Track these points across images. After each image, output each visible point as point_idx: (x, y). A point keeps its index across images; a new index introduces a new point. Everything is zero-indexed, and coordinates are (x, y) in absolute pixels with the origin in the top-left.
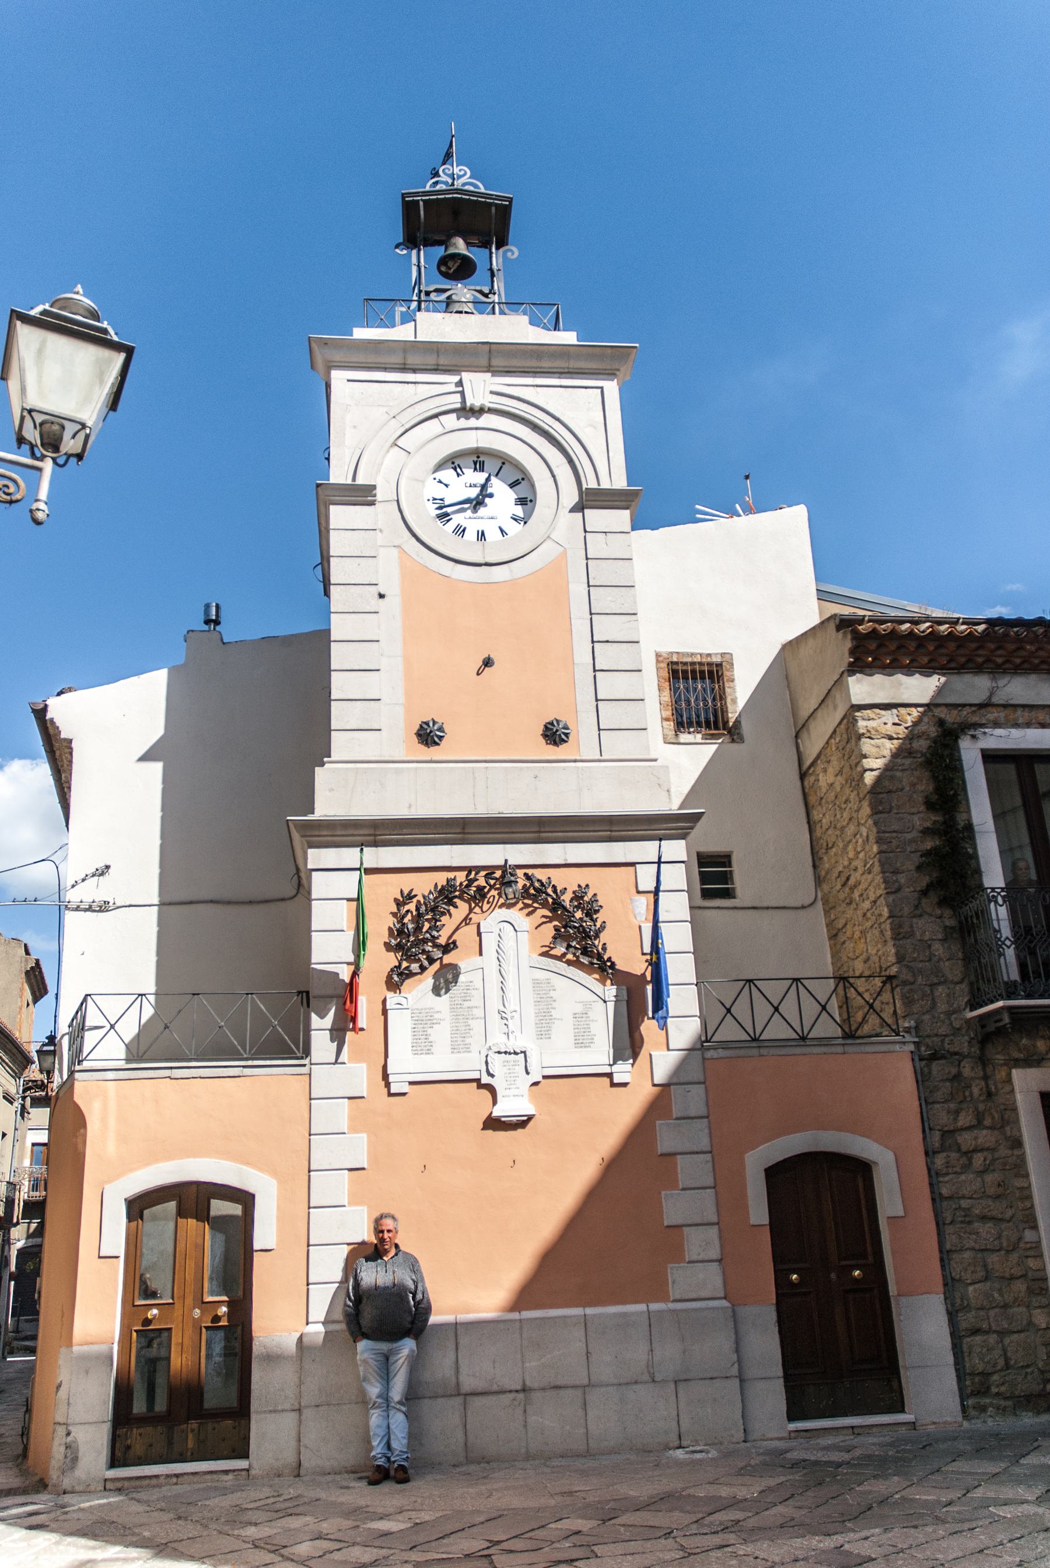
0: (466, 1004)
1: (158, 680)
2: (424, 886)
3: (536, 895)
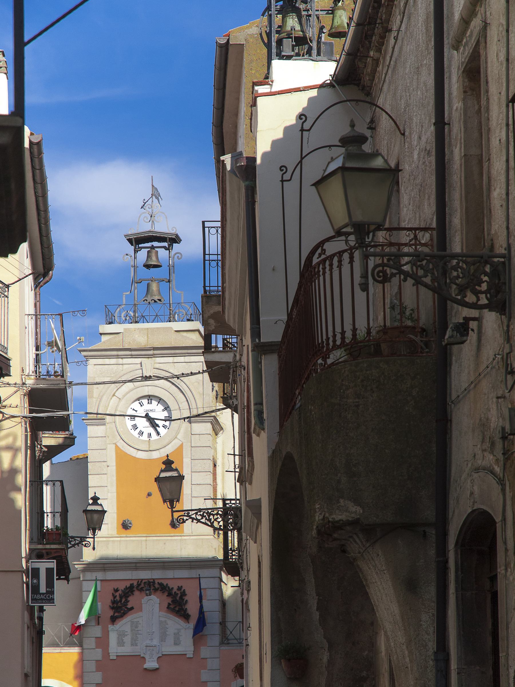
0: (136, 629)
2: (122, 586)
3: (162, 588)
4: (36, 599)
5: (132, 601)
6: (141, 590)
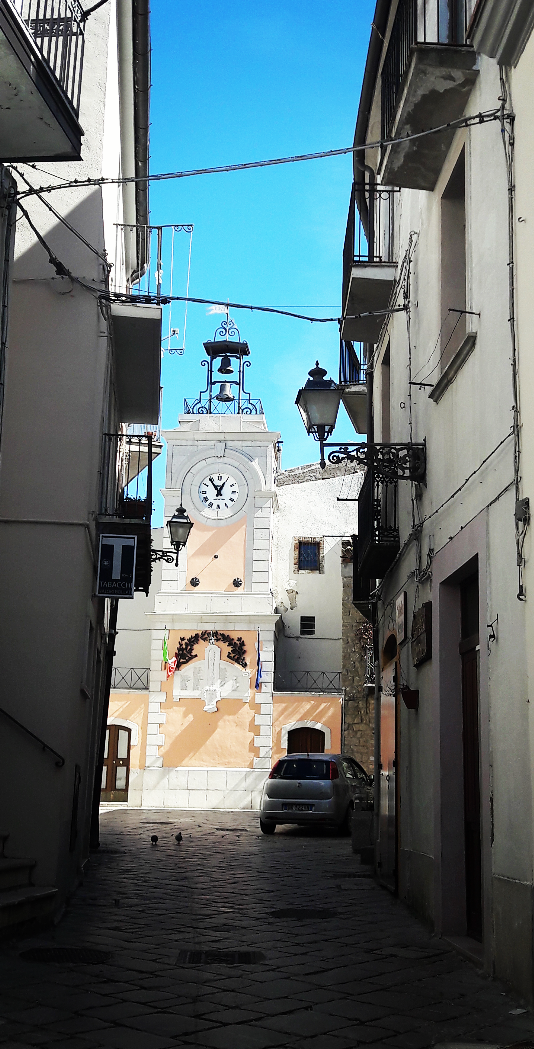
1: (100, 812)
4: (105, 588)
5: (197, 649)
6: (205, 640)
